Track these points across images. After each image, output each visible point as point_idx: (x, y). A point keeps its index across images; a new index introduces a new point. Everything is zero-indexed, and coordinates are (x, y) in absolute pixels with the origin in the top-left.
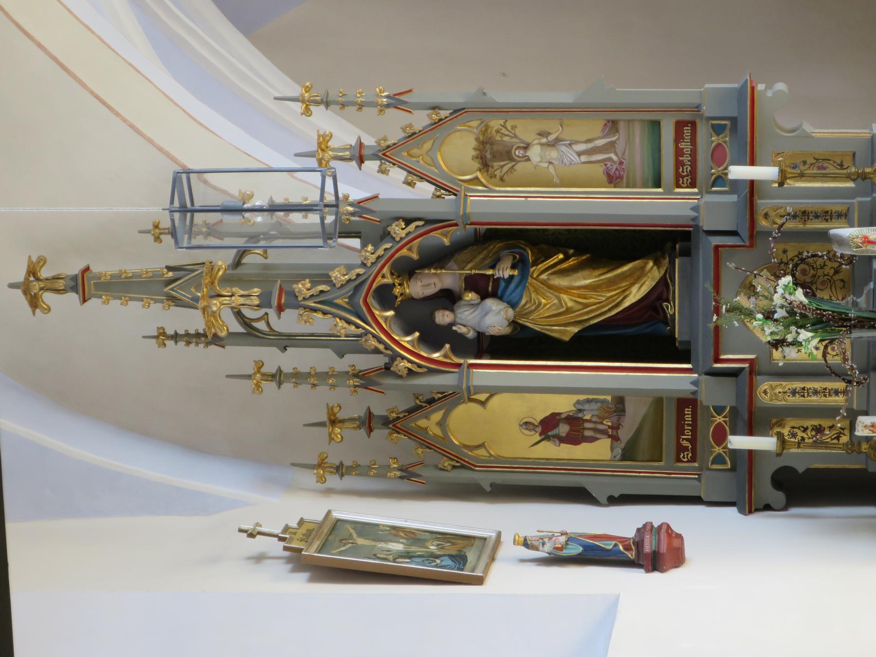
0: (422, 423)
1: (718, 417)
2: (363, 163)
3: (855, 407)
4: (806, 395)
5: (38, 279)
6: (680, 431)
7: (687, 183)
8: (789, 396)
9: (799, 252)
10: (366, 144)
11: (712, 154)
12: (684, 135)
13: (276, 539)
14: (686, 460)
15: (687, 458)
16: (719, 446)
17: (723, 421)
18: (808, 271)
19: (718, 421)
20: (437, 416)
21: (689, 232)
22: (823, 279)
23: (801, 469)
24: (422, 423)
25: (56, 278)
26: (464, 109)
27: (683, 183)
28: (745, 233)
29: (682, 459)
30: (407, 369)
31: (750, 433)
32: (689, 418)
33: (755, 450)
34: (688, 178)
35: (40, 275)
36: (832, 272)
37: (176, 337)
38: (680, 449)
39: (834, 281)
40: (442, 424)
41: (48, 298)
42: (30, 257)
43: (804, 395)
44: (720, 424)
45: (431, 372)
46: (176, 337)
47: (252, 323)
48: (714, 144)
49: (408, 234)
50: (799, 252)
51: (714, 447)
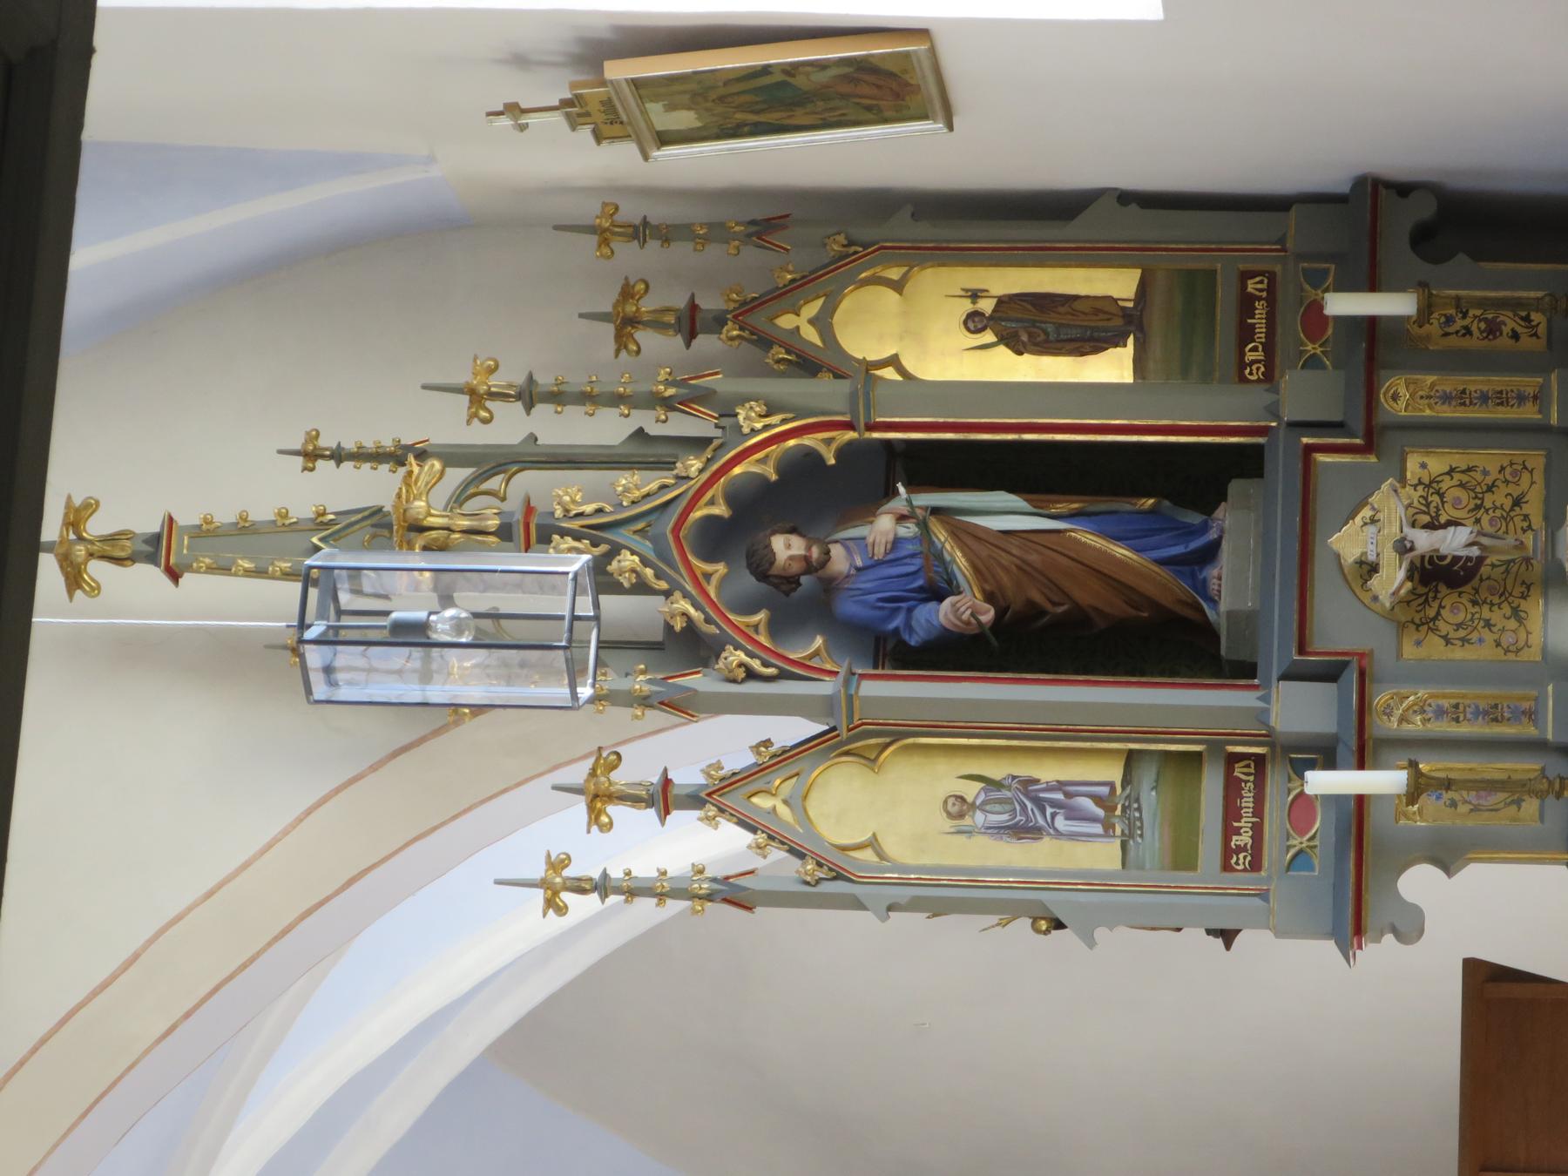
0: (786, 322)
1: (1299, 840)
2: (695, 338)
3: (1550, 736)
4: (1468, 402)
5: (81, 539)
6: (1229, 831)
7: (1244, 863)
8: (1436, 403)
9: (1451, 466)
10: (702, 307)
11: (1289, 815)
12: (1242, 812)
13: (523, 106)
14: (1241, 867)
15: (1244, 863)
16: (1313, 342)
17: (1322, 352)
18: (1460, 507)
19: (1311, 353)
20: (812, 309)
21: (1259, 449)
22: (1489, 517)
23: (1462, 259)
24: (786, 322)
25: (112, 539)
26: (877, 243)
27: (1237, 863)
28: (1359, 425)
29: (1248, 376)
30: (743, 669)
31: (1372, 322)
32: (1248, 813)
33: (1379, 316)
34: (1259, 365)
35: (84, 527)
36: (1508, 503)
37: (338, 456)
38: (1228, 852)
39: (1512, 518)
40: (823, 322)
41: (97, 570)
42: (69, 497)
43: (1458, 717)
44: (1314, 355)
45: (783, 675)
46: (338, 456)
47: (474, 470)
48: (1292, 852)
49: (766, 428)
50: (1451, 466)
51: (1302, 344)
